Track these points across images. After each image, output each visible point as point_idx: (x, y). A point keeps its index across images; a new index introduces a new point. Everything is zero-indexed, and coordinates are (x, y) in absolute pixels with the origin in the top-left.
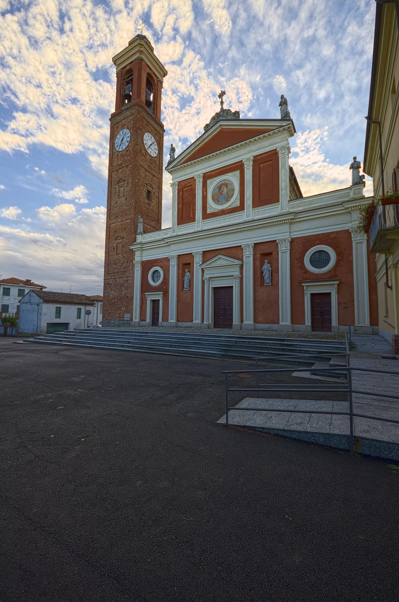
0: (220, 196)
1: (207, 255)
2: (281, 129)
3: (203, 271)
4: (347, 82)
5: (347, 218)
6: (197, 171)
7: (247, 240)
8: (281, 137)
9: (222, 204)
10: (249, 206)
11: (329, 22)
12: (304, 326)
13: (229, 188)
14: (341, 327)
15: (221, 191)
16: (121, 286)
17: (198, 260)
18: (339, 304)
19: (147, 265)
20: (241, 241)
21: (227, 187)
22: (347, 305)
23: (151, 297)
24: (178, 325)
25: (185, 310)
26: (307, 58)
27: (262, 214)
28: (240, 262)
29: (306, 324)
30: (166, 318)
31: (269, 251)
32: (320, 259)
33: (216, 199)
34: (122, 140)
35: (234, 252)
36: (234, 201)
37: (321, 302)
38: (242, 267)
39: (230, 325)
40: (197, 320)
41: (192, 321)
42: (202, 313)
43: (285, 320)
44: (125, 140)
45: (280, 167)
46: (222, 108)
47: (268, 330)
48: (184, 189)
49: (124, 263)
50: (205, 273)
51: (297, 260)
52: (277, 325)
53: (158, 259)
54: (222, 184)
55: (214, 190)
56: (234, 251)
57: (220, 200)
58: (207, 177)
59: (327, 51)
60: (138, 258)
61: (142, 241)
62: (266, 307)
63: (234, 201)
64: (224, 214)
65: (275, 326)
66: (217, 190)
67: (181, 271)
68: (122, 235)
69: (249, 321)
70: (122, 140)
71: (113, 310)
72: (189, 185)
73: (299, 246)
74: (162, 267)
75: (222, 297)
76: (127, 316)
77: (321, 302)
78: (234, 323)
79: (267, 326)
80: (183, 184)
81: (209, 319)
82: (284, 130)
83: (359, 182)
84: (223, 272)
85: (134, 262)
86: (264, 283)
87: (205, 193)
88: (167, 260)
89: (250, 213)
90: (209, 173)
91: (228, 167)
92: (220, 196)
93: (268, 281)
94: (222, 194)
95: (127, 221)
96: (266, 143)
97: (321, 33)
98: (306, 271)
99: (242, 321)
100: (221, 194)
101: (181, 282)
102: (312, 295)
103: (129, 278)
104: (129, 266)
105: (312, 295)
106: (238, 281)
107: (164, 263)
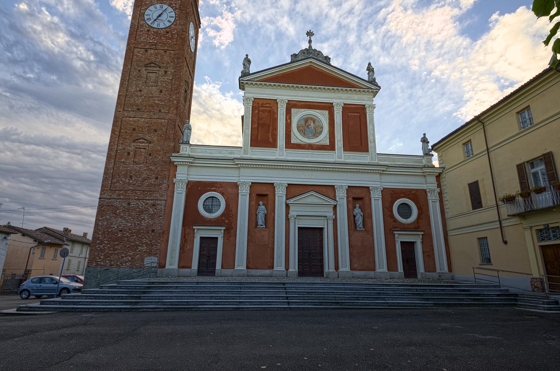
0: (306, 129)
1: (294, 190)
2: (370, 90)
3: (287, 206)
4: (353, 65)
5: (422, 180)
6: (283, 95)
7: (342, 182)
8: (368, 96)
9: (309, 138)
10: (340, 148)
11: (361, 21)
12: (397, 273)
13: (317, 124)
14: (427, 273)
15: (307, 124)
16: (141, 212)
17: (280, 193)
18: (423, 252)
19: (195, 190)
20: (368, 183)
21: (314, 122)
22: (429, 255)
23: (200, 233)
24: (249, 274)
25: (260, 254)
26: (336, 36)
27: (352, 159)
28: (333, 202)
29: (399, 271)
30: (229, 262)
31: (361, 196)
32: (405, 210)
33: (316, 134)
34: (160, 16)
35: (328, 190)
36: (323, 138)
37: (208, 244)
38: (335, 207)
39: (320, 272)
40: (279, 267)
41: (273, 267)
42: (285, 258)
43: (381, 266)
44: (164, 17)
45: (368, 122)
46: (310, 47)
47: (365, 277)
48: (261, 108)
49: (148, 178)
50: (291, 208)
51: (387, 208)
52: (373, 272)
53: (220, 183)
54: (308, 118)
55: (299, 121)
56: (324, 189)
57: (306, 133)
58: (291, 105)
59: (352, 39)
60: (183, 175)
61: (190, 154)
62: (362, 253)
63: (323, 138)
64: (312, 149)
65: (371, 273)
66: (303, 122)
67: (253, 202)
68: (147, 137)
69: (345, 267)
70: (160, 16)
71: (115, 250)
72: (268, 105)
73: (390, 195)
74: (223, 194)
75: (310, 241)
76: (150, 261)
77: (208, 244)
78: (326, 270)
79: (363, 273)
80: (261, 102)
81: (294, 267)
82: (372, 92)
83: (427, 154)
84: (310, 211)
85: (175, 180)
86: (360, 229)
87: (289, 121)
88: (235, 186)
89: (339, 155)
90: (295, 102)
91: (316, 104)
92: (306, 129)
93: (361, 226)
94: (307, 126)
95: (160, 121)
96: (356, 96)
97: (354, 25)
98: (395, 220)
99: (337, 268)
100: (308, 127)
101: (254, 217)
102: (201, 238)
103: (159, 202)
104: (160, 184)
105: (201, 238)
106: (331, 223)
107: (230, 190)
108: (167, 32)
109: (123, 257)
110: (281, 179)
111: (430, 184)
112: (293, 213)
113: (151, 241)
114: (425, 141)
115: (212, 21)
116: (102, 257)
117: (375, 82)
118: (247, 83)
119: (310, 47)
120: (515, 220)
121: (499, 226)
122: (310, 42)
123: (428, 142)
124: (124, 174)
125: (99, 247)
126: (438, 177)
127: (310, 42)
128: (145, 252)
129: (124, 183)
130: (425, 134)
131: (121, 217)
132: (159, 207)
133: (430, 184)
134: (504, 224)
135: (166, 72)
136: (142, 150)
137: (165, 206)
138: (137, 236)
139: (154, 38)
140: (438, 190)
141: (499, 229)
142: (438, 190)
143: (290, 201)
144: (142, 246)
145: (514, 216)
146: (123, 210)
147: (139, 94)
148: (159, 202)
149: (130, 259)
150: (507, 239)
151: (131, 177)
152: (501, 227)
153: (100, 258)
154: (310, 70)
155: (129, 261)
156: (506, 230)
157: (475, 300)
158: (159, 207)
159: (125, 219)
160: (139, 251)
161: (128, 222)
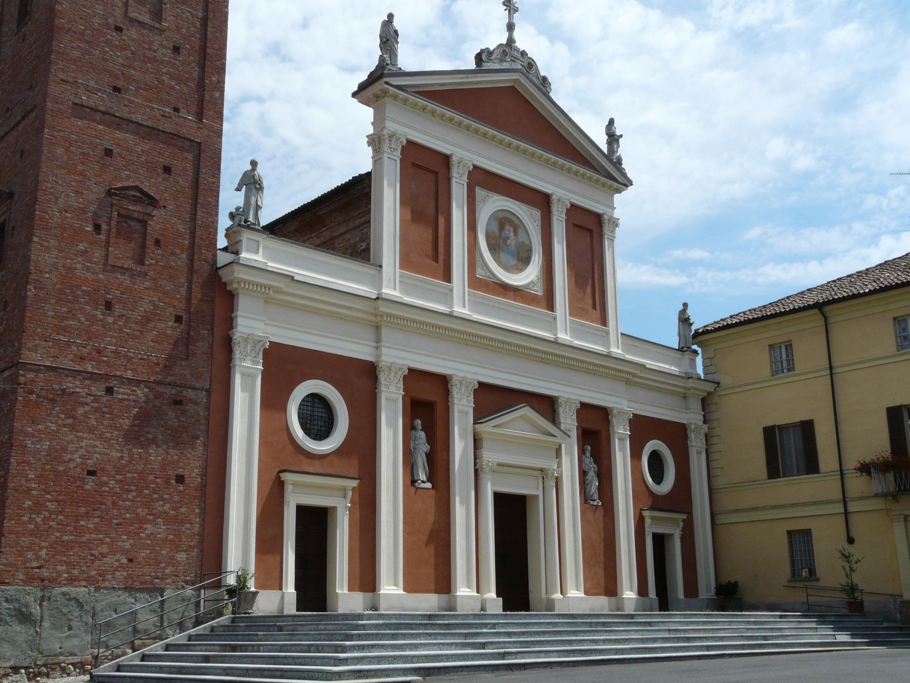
1: (493, 399)
54: (505, 219)
93: (596, 496)
103: (190, 394)
110: (466, 370)
111: (691, 417)
112: (490, 456)
113: (176, 509)
114: (684, 320)
116: (43, 553)
117: (621, 164)
118: (395, 97)
119: (511, 41)
120: (878, 504)
121: (842, 511)
122: (511, 27)
123: (691, 324)
124: (88, 294)
126: (705, 402)
127: (511, 27)
128: (165, 540)
129: (92, 319)
130: (254, 164)
131: (91, 430)
132: (190, 407)
133: (691, 417)
134: (852, 507)
136: (132, 223)
137: (208, 408)
138: (140, 492)
140: (705, 428)
141: (843, 516)
142: (705, 428)
143: (483, 428)
144: (153, 522)
145: (877, 495)
146: (97, 410)
148: (190, 394)
149: (125, 561)
150: (855, 534)
151: (109, 305)
152: (846, 513)
153: (38, 558)
155: (121, 567)
156: (853, 519)
158: (190, 407)
159: (101, 437)
161: (111, 447)
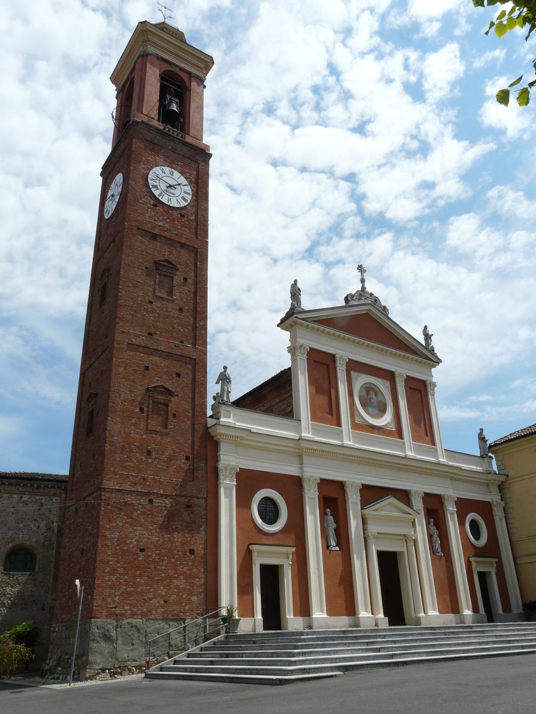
1: (372, 494)
35: (404, 496)
93: (439, 550)
103: (195, 501)
108: (182, 216)
109: (150, 599)
110: (354, 478)
111: (493, 497)
112: (372, 529)
113: (190, 570)
114: (482, 439)
115: (113, 196)
116: (117, 599)
118: (301, 325)
119: (363, 288)
122: (363, 281)
123: (486, 441)
125: (110, 579)
126: (501, 488)
127: (363, 281)
128: (185, 589)
131: (141, 525)
135: (185, 279)
136: (161, 406)
138: (169, 560)
139: (163, 220)
147: (148, 306)
149: (162, 602)
153: (114, 602)
154: (366, 320)
155: (160, 606)
157: (433, 646)
158: (196, 509)
159: (147, 529)
160: (175, 587)
